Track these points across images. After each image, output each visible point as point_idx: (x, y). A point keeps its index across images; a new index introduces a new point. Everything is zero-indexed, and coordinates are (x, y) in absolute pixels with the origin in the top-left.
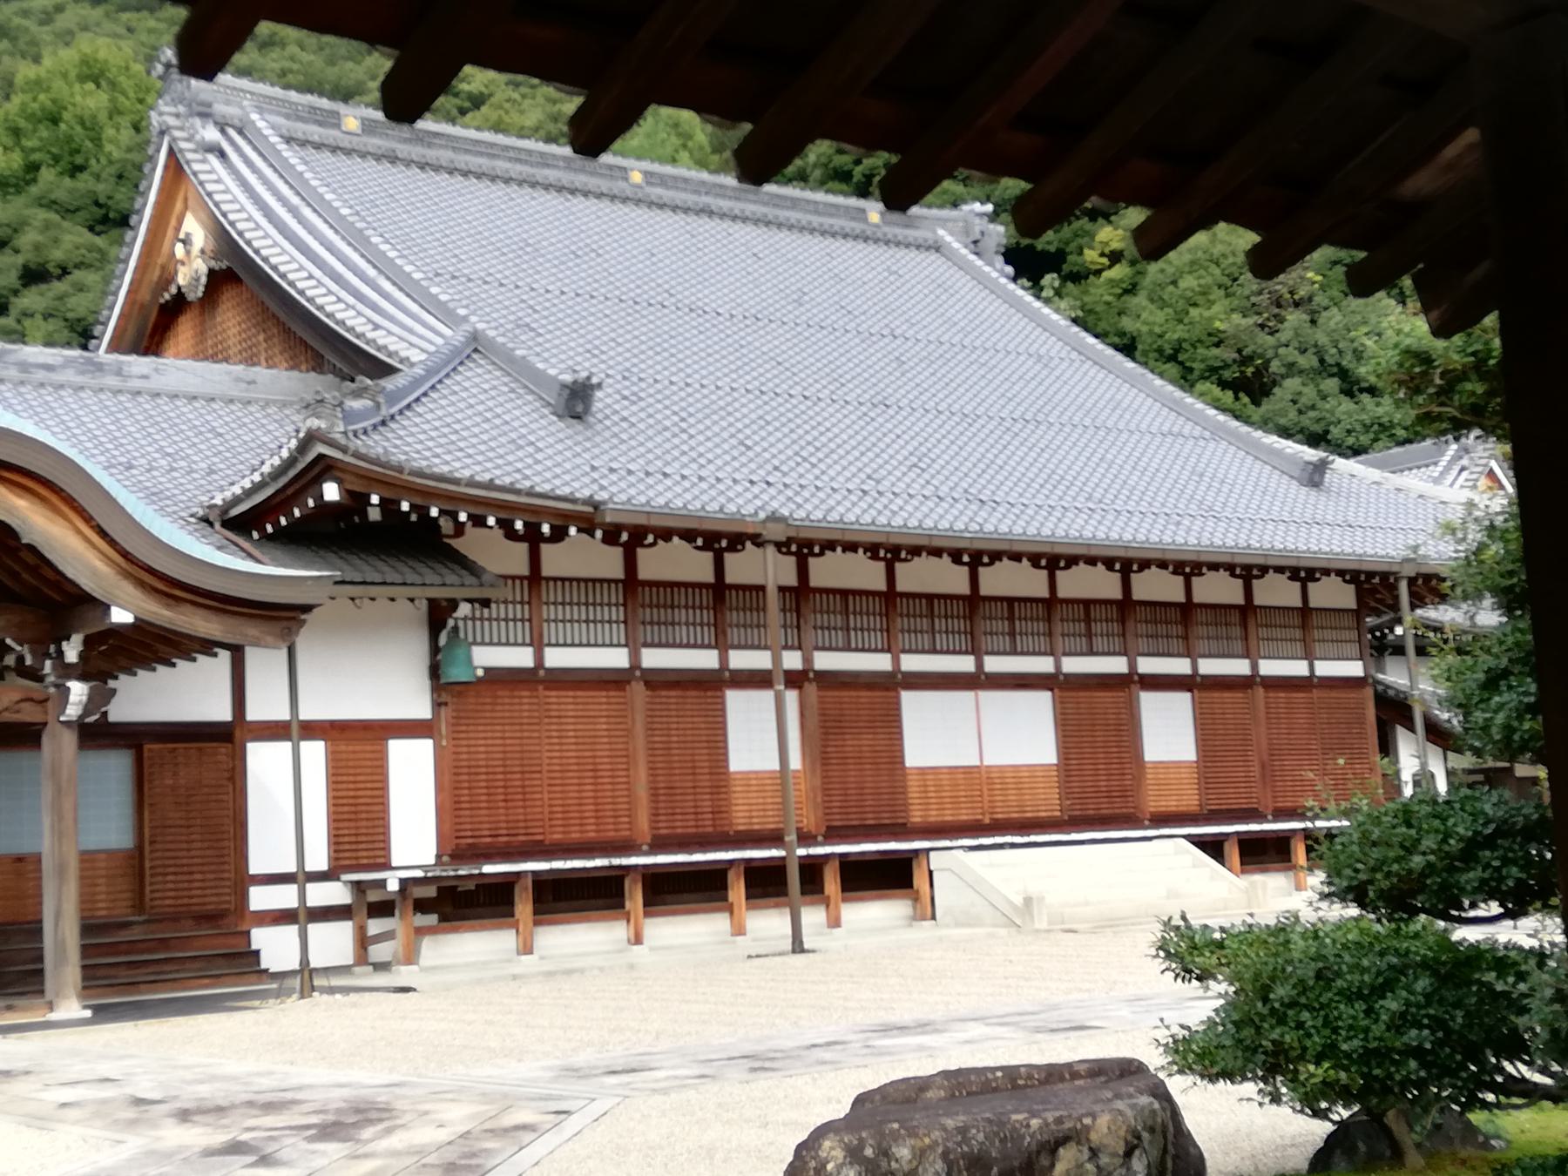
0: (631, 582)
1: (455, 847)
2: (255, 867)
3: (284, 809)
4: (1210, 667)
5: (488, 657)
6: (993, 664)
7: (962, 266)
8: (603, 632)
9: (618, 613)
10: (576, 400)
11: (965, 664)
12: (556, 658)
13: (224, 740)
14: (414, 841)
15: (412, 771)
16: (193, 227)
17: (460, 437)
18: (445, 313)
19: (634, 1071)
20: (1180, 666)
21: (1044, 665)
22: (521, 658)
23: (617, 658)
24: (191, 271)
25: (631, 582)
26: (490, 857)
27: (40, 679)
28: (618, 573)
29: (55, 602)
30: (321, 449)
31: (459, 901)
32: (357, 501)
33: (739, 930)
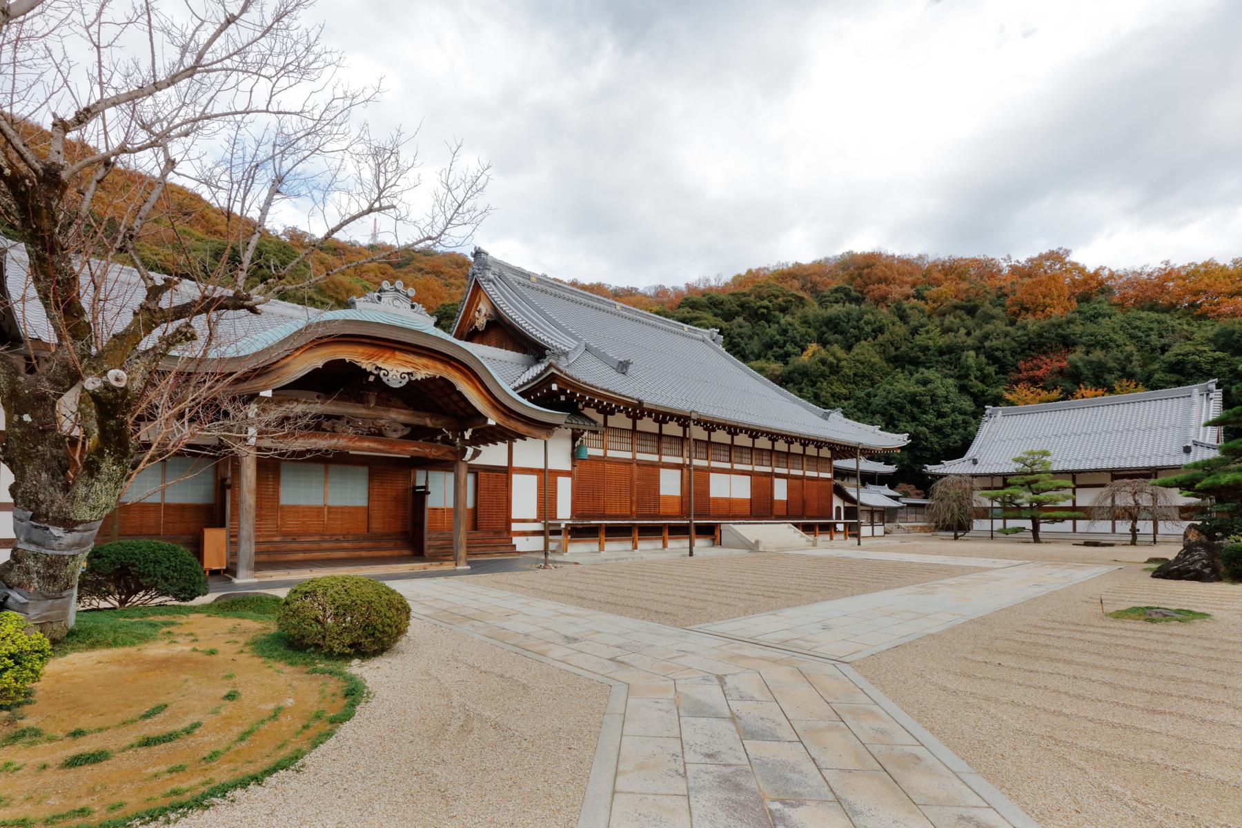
0: (634, 431)
1: (575, 513)
2: (514, 516)
3: (524, 498)
4: (793, 472)
5: (592, 452)
6: (737, 467)
7: (710, 346)
8: (625, 446)
9: (629, 441)
10: (623, 367)
11: (728, 466)
12: (611, 454)
13: (505, 473)
14: (564, 510)
15: (564, 487)
16: (484, 307)
17: (592, 374)
18: (576, 338)
19: (1096, 544)
20: (785, 471)
21: (749, 468)
22: (600, 453)
23: (629, 455)
24: (481, 322)
25: (634, 431)
26: (594, 518)
27: (455, 445)
28: (630, 427)
29: (466, 415)
30: (553, 370)
31: (578, 532)
32: (562, 391)
33: (665, 546)
